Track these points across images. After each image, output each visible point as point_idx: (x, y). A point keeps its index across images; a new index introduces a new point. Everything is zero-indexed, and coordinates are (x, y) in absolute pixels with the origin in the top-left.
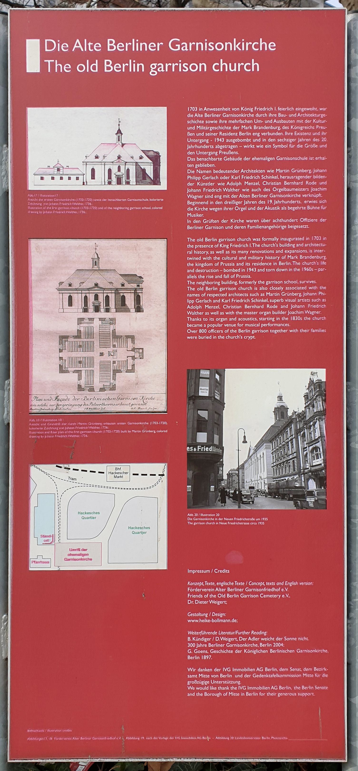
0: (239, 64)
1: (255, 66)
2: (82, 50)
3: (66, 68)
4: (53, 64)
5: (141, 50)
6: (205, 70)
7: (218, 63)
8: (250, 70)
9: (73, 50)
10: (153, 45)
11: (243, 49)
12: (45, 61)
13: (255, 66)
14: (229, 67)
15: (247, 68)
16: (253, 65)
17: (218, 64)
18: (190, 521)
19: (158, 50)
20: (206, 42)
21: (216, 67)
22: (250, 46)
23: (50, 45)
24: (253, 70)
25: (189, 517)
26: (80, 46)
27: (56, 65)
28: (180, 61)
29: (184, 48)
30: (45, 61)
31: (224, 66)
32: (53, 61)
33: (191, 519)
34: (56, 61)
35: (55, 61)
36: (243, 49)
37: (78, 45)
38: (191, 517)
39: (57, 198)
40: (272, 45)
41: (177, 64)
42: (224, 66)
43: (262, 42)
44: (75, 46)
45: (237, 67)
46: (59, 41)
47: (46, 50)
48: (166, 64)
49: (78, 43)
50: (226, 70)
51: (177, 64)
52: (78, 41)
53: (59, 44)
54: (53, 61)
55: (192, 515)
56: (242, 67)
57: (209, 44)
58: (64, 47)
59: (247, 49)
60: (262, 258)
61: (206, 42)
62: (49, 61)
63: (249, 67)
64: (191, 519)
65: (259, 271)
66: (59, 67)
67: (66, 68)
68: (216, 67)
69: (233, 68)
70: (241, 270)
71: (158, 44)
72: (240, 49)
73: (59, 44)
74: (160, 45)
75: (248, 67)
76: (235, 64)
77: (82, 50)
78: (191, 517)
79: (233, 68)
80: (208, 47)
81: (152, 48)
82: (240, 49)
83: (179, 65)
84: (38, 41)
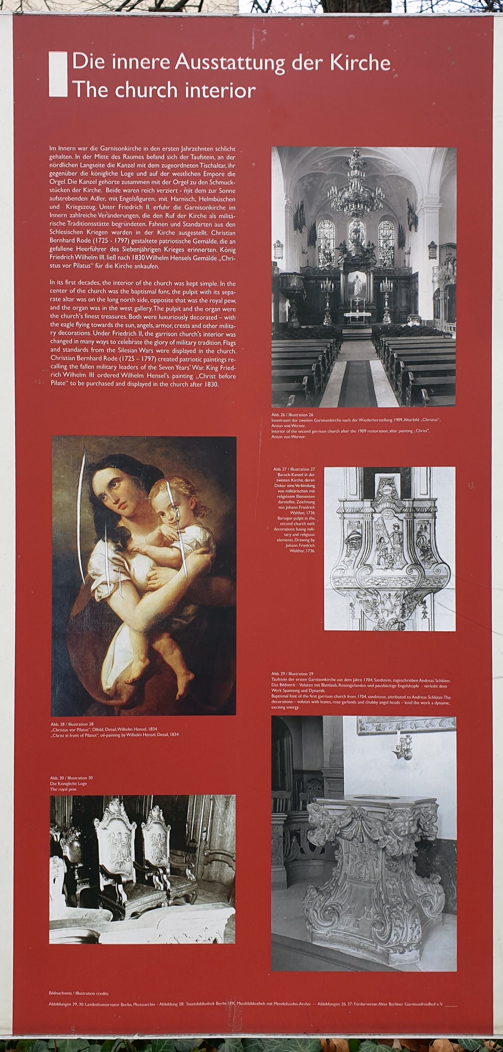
0: (150, 88)
1: (172, 91)
2: (188, 68)
3: (101, 92)
4: (83, 87)
5: (119, 67)
6: (176, 96)
7: (123, 86)
8: (123, 96)
9: (176, 68)
10: (146, 61)
11: (347, 68)
12: (74, 82)
13: (172, 91)
14: (137, 92)
15: (119, 93)
16: (127, 89)
17: (164, 88)
18: (53, 786)
19: (153, 67)
20: (348, 58)
21: (121, 92)
22: (356, 64)
23: (80, 60)
24: (127, 96)
25: (52, 780)
26: (186, 63)
27: (88, 88)
28: (231, 84)
29: (231, 66)
30: (74, 82)
31: (131, 90)
32: (84, 82)
33: (55, 784)
34: (88, 82)
35: (86, 82)
36: (347, 68)
37: (182, 60)
38: (55, 781)
39: (312, 677)
40: (99, 61)
41: (227, 88)
42: (131, 90)
43: (373, 59)
44: (179, 63)
45: (148, 92)
46: (91, 55)
47: (75, 67)
48: (249, 88)
49: (182, 58)
50: (134, 96)
51: (227, 88)
52: (182, 55)
53: (92, 59)
54: (84, 82)
55: (56, 778)
56: (155, 92)
57: (204, 61)
58: (98, 63)
59: (352, 68)
60: (115, 368)
61: (348, 58)
62: (79, 82)
63: (164, 92)
64: (55, 784)
65: (117, 385)
66: (92, 90)
67: (101, 92)
68: (121, 92)
69: (142, 93)
70: (152, 384)
71: (317, 62)
72: (342, 69)
73: (92, 59)
74: (319, 63)
75: (163, 92)
76: (146, 88)
77: (188, 68)
78: (55, 781)
79: (142, 93)
80: (202, 64)
81: (308, 66)
82: (342, 69)
83: (230, 89)
84: (65, 54)
